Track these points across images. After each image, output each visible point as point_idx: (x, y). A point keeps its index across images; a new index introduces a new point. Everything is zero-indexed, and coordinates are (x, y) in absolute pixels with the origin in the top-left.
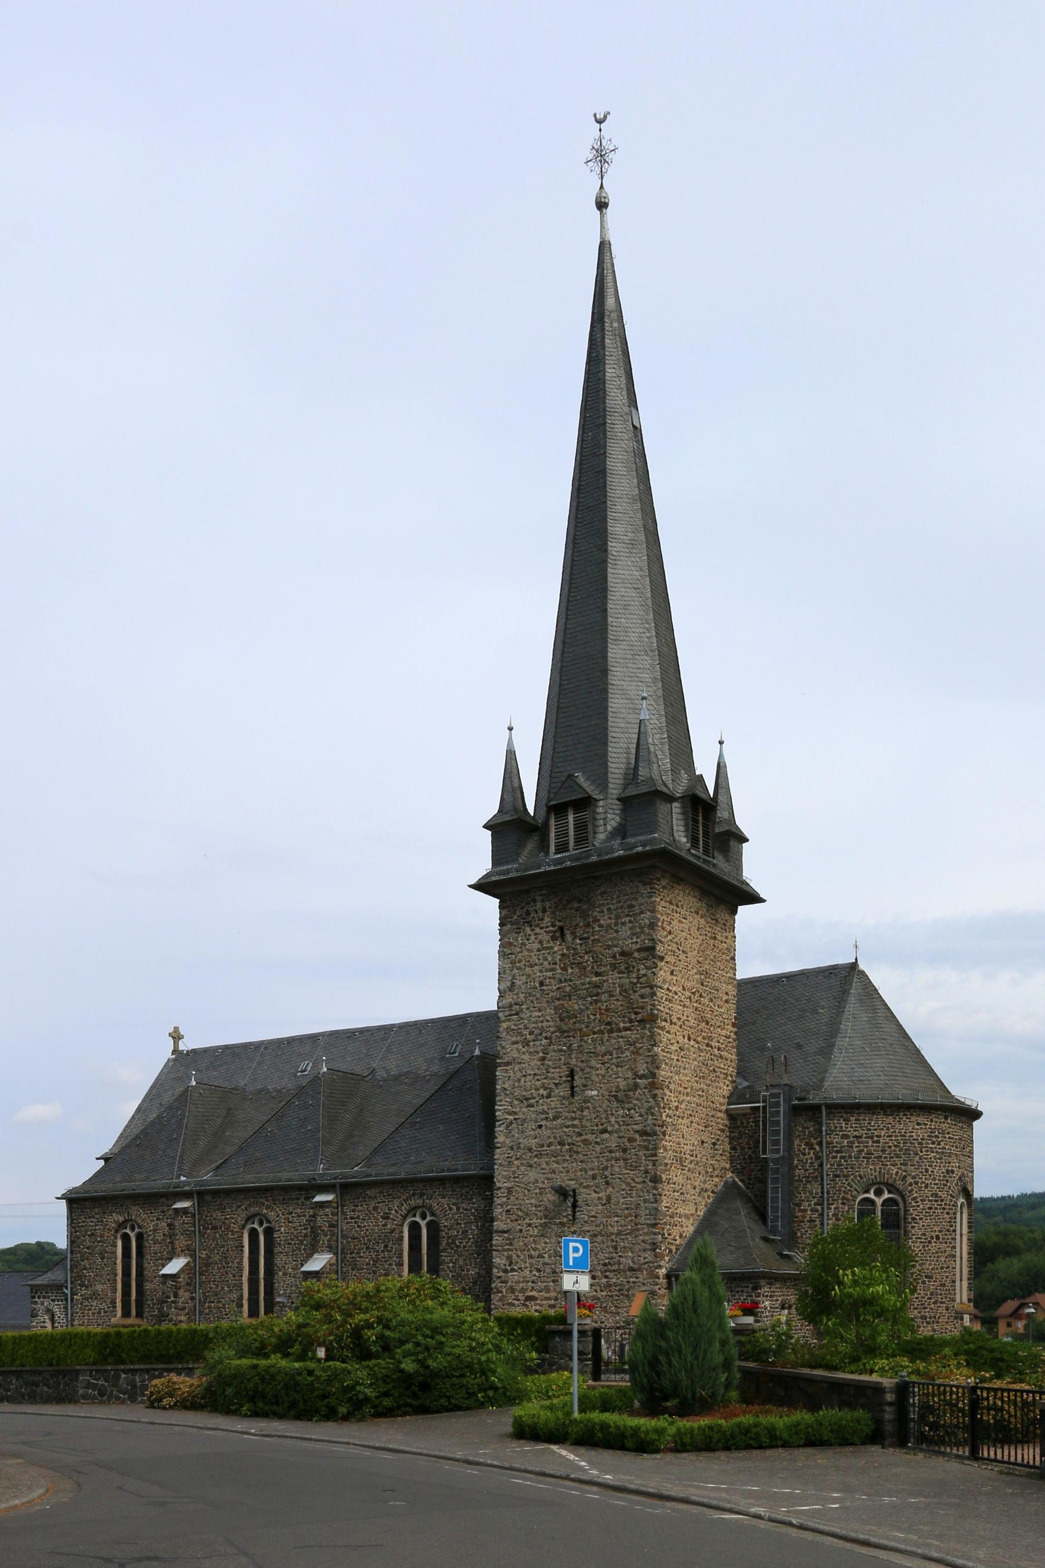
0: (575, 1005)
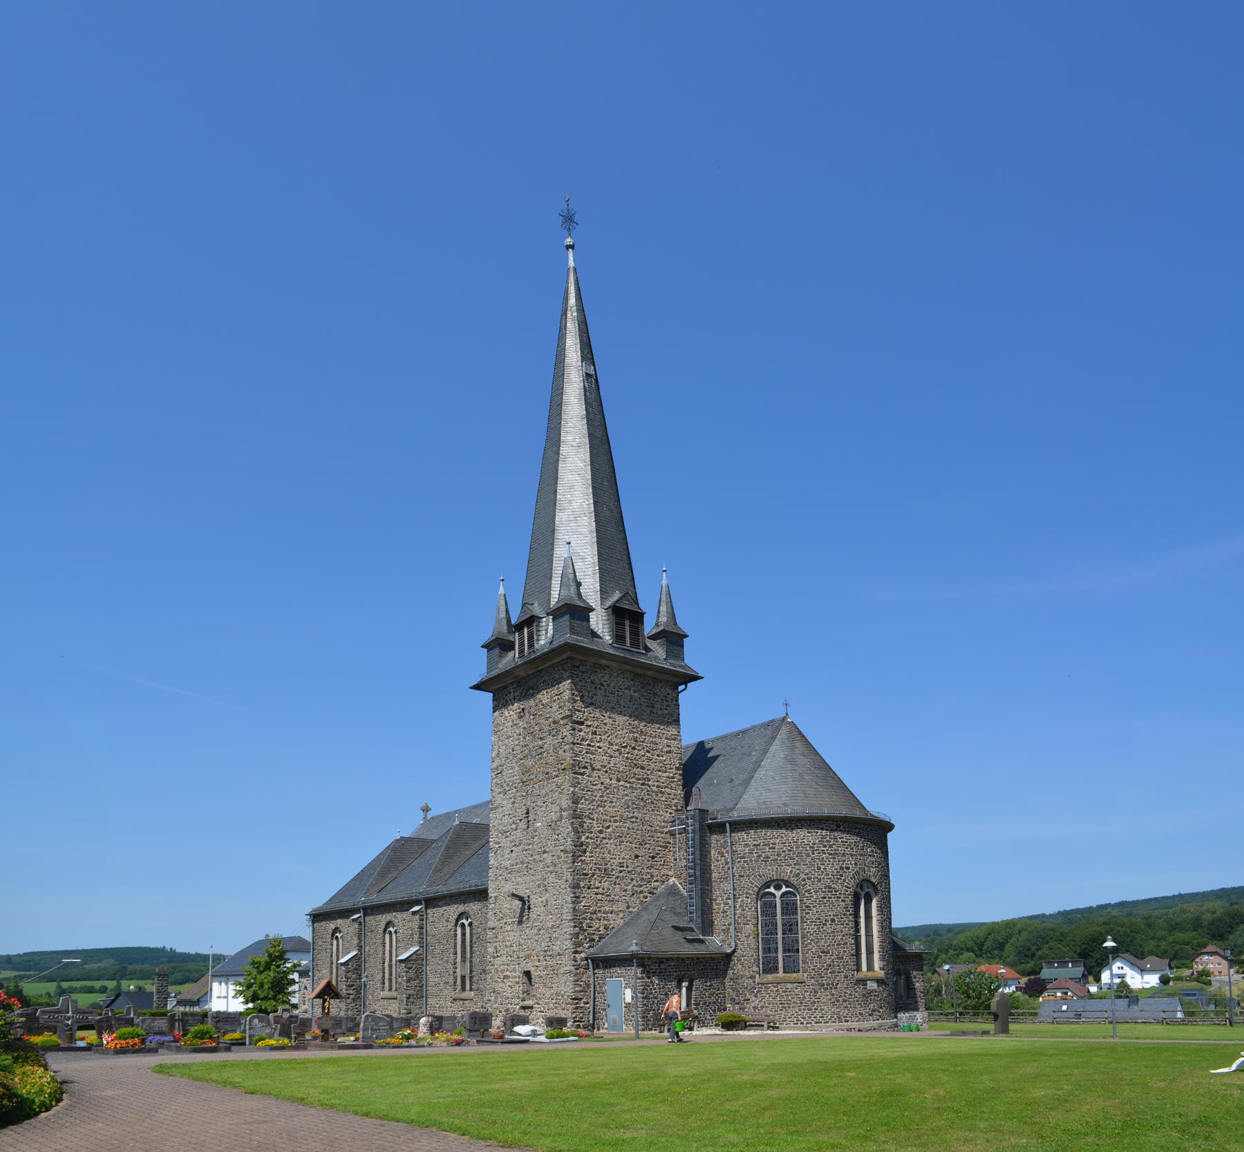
0: (529, 763)
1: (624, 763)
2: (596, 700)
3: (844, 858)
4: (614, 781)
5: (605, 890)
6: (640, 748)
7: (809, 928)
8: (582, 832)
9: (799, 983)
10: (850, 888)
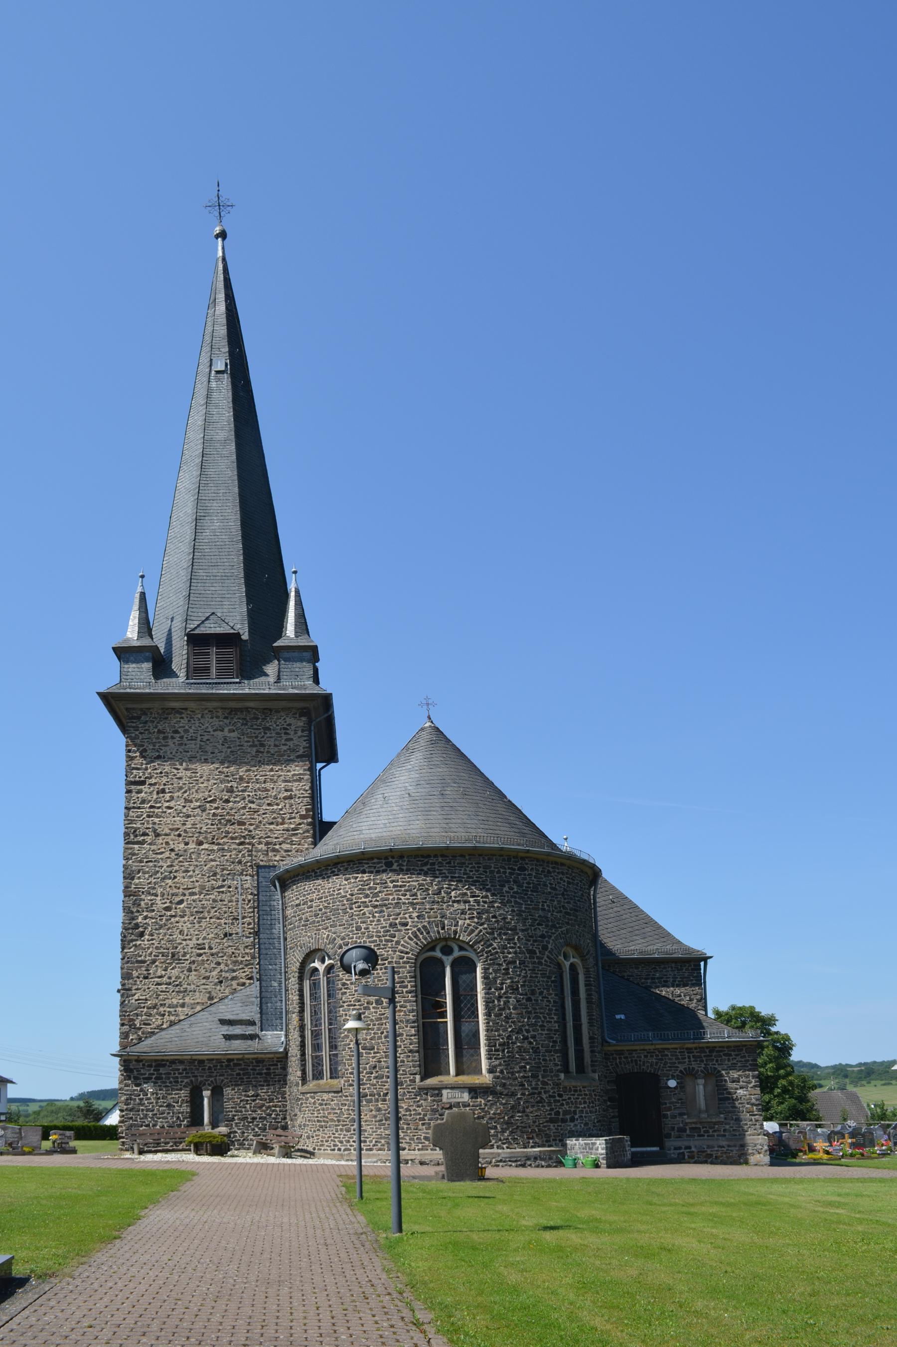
1: (210, 822)
2: (166, 752)
3: (397, 910)
4: (192, 846)
5: (173, 979)
6: (238, 799)
7: (346, 1015)
8: (138, 911)
9: (335, 1092)
10: (407, 953)
